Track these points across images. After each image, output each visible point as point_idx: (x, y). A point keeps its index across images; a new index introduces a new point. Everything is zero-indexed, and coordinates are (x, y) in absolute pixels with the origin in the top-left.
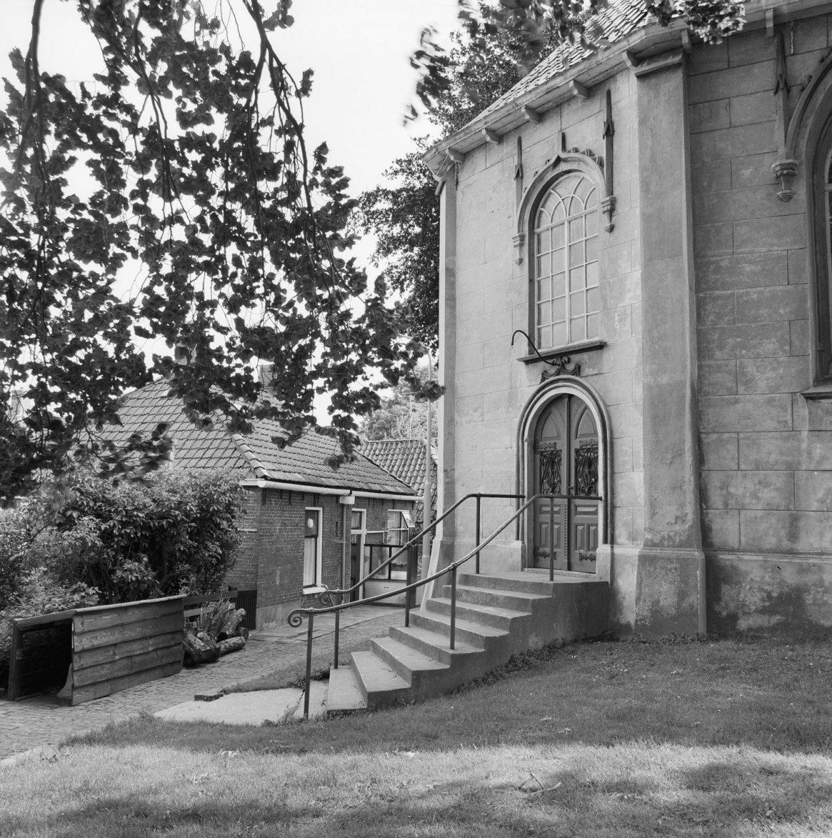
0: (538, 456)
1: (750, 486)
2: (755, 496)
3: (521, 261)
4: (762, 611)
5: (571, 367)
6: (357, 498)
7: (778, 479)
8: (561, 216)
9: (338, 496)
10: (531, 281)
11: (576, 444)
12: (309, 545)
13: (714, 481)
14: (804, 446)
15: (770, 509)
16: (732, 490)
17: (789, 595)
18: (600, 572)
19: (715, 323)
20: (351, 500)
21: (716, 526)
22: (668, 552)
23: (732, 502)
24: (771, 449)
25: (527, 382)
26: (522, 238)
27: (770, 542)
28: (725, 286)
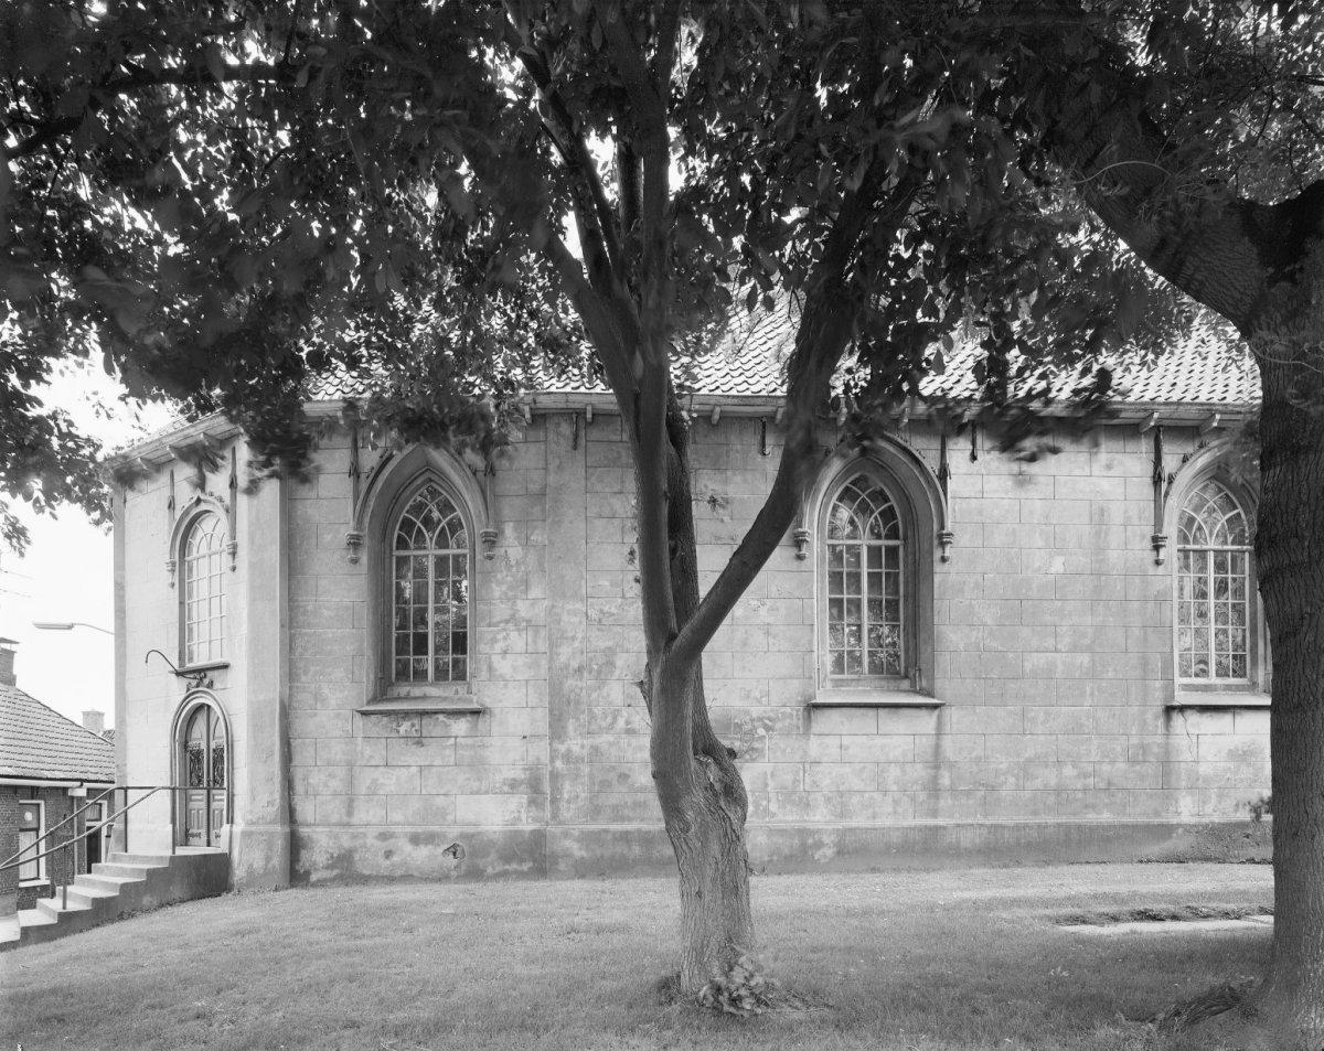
0: (188, 755)
1: (323, 777)
2: (326, 785)
3: (173, 585)
4: (327, 867)
5: (206, 681)
6: (88, 789)
7: (341, 772)
8: (204, 550)
9: (65, 789)
10: (182, 603)
11: (213, 746)
12: (26, 840)
13: (298, 774)
14: (359, 748)
15: (335, 794)
16: (311, 781)
17: (344, 856)
18: (220, 847)
19: (301, 654)
20: (82, 792)
21: (299, 808)
22: (262, 828)
23: (310, 790)
24: (337, 750)
25: (177, 689)
26: (173, 564)
27: (335, 818)
28: (309, 626)
